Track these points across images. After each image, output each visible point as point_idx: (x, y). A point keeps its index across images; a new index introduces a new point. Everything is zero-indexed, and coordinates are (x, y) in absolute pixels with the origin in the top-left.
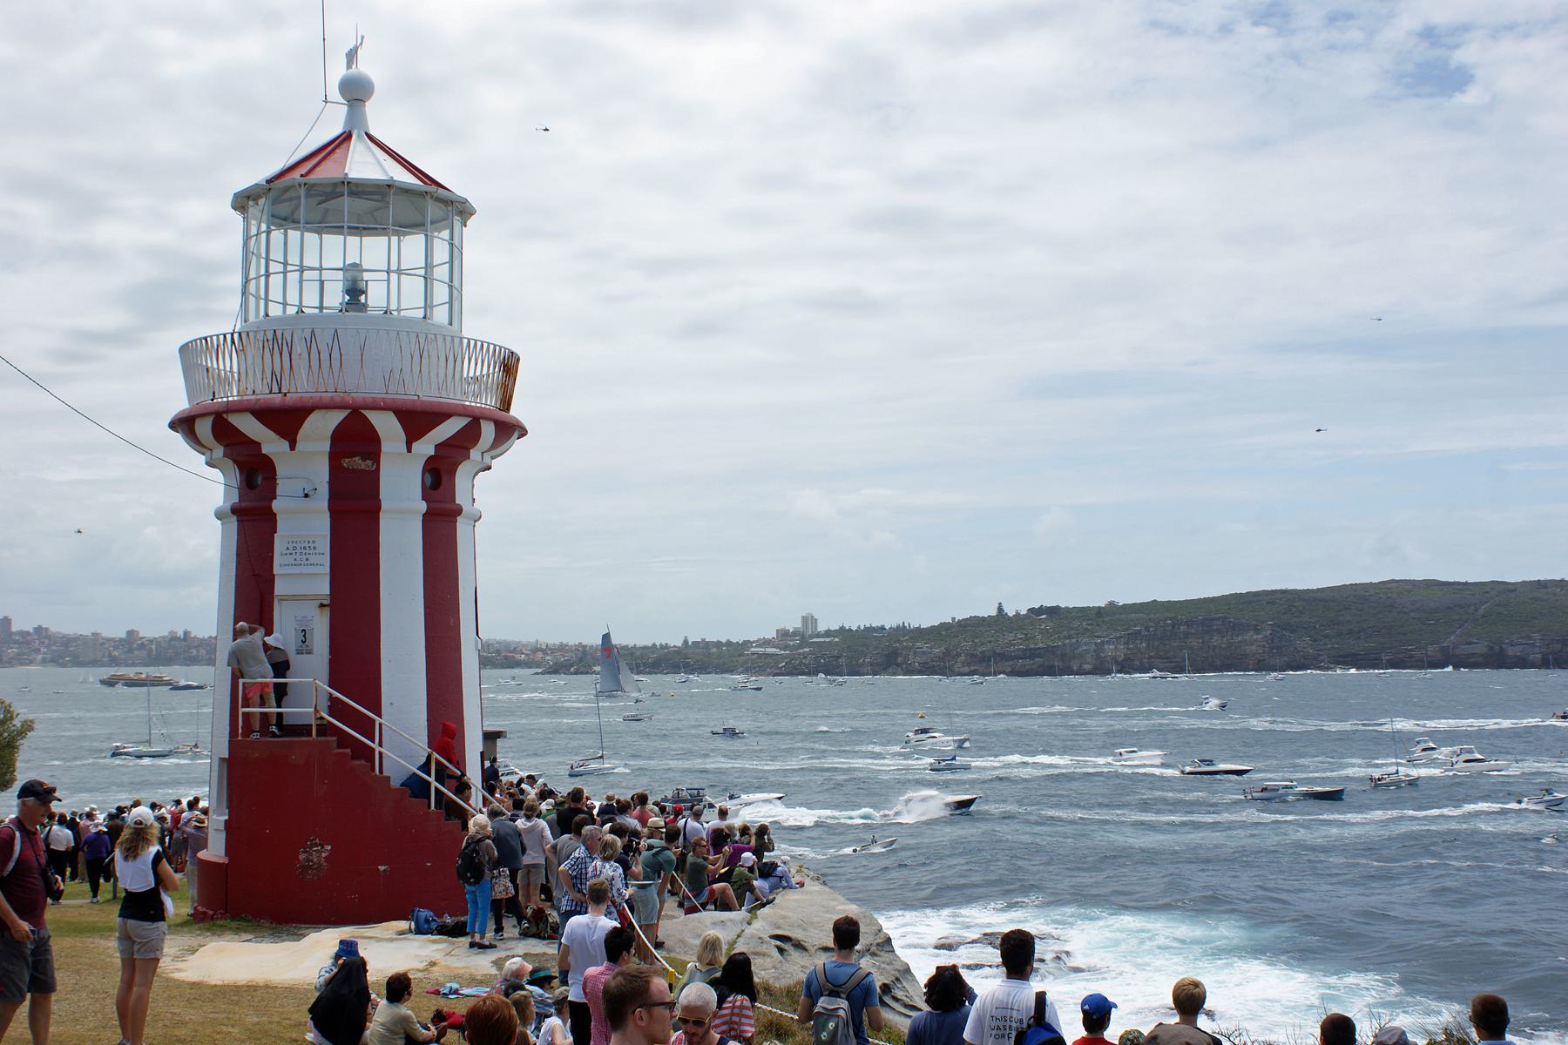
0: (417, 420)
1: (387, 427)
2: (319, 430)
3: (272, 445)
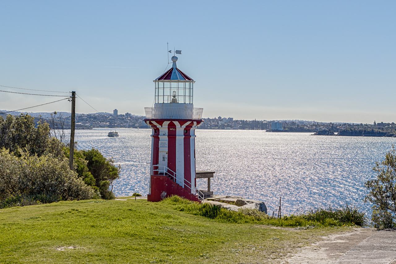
0: (182, 122)
1: (176, 123)
2: (166, 124)
3: (158, 126)
